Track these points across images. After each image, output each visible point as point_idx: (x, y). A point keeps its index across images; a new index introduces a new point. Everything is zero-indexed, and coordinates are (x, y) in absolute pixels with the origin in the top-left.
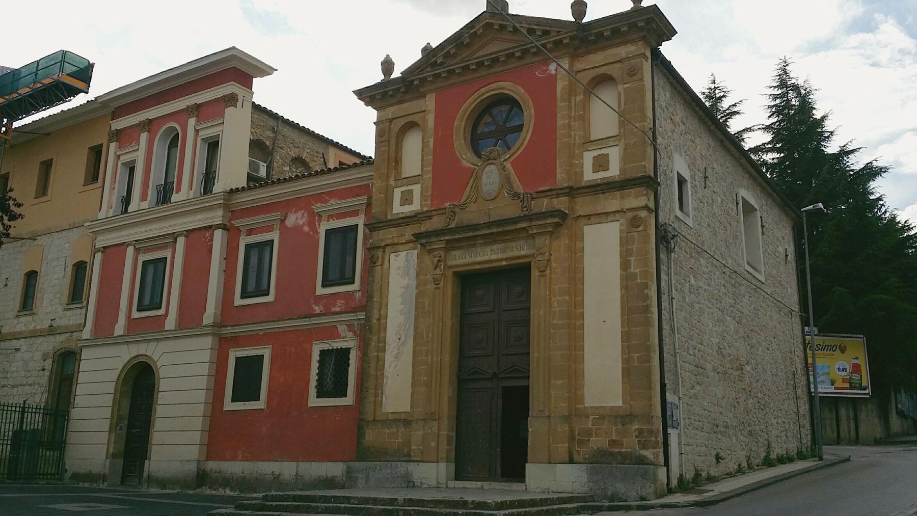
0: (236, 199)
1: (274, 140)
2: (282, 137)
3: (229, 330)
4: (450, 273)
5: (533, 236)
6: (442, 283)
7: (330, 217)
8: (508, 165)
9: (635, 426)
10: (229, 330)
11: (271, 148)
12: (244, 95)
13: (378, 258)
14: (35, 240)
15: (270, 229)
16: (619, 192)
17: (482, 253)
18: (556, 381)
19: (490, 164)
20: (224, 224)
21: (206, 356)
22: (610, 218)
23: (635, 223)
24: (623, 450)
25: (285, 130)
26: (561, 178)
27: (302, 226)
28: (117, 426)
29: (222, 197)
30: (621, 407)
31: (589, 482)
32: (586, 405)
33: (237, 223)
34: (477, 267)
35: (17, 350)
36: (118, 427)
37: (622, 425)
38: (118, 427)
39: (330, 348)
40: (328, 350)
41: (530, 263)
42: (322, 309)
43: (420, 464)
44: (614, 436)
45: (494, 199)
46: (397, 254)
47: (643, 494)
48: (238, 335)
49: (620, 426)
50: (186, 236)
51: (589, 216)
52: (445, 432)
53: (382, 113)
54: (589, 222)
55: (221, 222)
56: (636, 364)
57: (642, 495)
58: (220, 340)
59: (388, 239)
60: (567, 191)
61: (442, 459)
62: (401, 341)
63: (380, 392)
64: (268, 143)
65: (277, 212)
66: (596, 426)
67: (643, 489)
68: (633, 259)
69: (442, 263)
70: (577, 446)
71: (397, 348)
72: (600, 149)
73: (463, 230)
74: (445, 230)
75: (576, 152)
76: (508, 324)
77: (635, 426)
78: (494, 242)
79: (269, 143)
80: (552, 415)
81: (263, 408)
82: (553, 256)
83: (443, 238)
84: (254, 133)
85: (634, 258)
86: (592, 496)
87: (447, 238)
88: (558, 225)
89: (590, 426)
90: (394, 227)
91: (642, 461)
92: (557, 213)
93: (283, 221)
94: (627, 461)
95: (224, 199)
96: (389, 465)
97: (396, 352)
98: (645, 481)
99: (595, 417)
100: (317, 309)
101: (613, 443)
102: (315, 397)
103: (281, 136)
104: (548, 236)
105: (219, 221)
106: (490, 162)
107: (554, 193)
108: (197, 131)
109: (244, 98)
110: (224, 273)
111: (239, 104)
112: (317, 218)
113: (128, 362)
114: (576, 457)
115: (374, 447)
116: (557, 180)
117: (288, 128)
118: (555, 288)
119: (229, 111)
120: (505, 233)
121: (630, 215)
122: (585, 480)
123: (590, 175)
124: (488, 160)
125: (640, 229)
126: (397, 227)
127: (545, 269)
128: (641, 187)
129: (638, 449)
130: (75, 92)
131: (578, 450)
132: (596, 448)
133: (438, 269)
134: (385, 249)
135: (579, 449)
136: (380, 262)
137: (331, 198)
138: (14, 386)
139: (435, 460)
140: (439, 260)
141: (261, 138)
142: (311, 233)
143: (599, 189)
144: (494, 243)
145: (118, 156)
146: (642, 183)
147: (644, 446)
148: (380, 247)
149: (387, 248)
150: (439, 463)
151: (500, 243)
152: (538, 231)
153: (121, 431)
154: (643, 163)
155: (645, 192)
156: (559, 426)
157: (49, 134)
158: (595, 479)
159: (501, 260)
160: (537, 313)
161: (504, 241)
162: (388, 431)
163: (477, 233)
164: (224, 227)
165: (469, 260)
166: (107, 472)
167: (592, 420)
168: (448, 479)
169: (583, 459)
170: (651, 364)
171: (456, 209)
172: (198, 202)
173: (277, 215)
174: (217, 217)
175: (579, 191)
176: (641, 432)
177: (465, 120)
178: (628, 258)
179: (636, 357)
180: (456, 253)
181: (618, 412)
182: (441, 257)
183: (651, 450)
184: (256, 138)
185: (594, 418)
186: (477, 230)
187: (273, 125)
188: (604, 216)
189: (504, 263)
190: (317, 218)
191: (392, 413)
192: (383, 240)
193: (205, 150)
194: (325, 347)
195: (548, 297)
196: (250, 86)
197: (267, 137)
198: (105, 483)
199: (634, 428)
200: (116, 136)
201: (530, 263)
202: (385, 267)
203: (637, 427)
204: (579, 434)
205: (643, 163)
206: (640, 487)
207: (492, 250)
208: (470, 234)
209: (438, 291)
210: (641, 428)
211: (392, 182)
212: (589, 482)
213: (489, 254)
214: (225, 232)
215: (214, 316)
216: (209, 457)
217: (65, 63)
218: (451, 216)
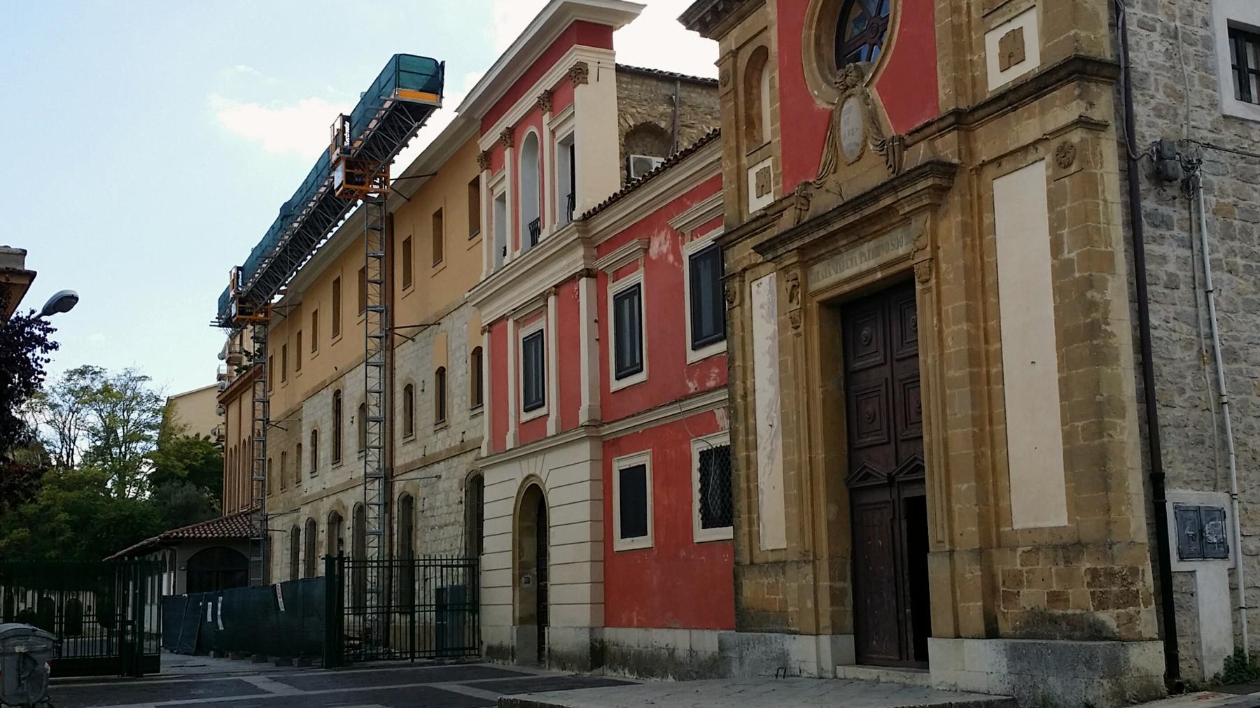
0: (594, 228)
1: (674, 117)
2: (689, 110)
3: (606, 430)
4: (813, 305)
5: (907, 218)
6: (802, 325)
7: (694, 234)
8: (873, 92)
9: (1086, 564)
10: (606, 430)
11: (670, 131)
12: (598, 61)
13: (735, 293)
14: (439, 324)
15: (633, 268)
16: (1036, 102)
17: (849, 263)
18: (959, 486)
19: (849, 96)
20: (587, 269)
21: (584, 472)
22: (1031, 158)
23: (1064, 158)
24: (1070, 612)
25: (693, 95)
26: (946, 98)
27: (667, 254)
28: (520, 578)
29: (575, 228)
30: (1065, 527)
31: (1010, 673)
32: (1015, 527)
33: (600, 265)
34: (847, 288)
35: (439, 477)
36: (523, 580)
37: (1066, 562)
38: (523, 580)
39: (710, 448)
40: (708, 450)
41: (912, 268)
42: (696, 385)
43: (797, 636)
44: (1054, 585)
45: (858, 160)
46: (759, 281)
47: (1090, 699)
48: (619, 435)
49: (1062, 566)
50: (555, 294)
51: (998, 160)
52: (826, 583)
53: (725, 44)
54: (1000, 171)
55: (583, 267)
56: (1082, 442)
57: (1087, 700)
58: (604, 446)
59: (744, 258)
60: (952, 119)
61: (825, 628)
62: (774, 429)
63: (755, 516)
64: (663, 125)
65: (632, 239)
66: (1027, 565)
67: (1090, 690)
68: (1065, 231)
69: (799, 290)
70: (1002, 605)
71: (769, 441)
72: (1009, 21)
73: (811, 227)
74: (797, 228)
75: (974, 37)
76: (904, 384)
77: (1086, 564)
78: (862, 240)
79: (666, 125)
80: (958, 548)
81: (650, 546)
82: (941, 249)
83: (791, 247)
84: (636, 115)
85: (1067, 229)
86: (1014, 699)
87: (796, 244)
88: (941, 192)
89: (1019, 567)
90: (749, 237)
91: (1097, 632)
92: (928, 168)
93: (646, 251)
94: (1078, 634)
95: (578, 231)
96: (763, 639)
97: (768, 449)
98: (1091, 673)
99: (1025, 549)
100: (692, 386)
101: (1055, 598)
102: (701, 526)
103: (686, 108)
104: (928, 214)
105: (580, 266)
106: (848, 93)
107: (934, 128)
108: (553, 132)
109: (600, 65)
110: (597, 343)
111: (591, 77)
112: (680, 238)
113: (522, 486)
114: (1004, 627)
115: (753, 608)
116: (940, 103)
117: (700, 90)
118: (948, 310)
119: (580, 92)
120: (870, 219)
121: (1055, 143)
122: (1004, 670)
123: (998, 80)
124: (846, 90)
125: (1073, 168)
126: (753, 236)
127: (928, 277)
128: (1069, 82)
129: (1092, 609)
130: (422, 113)
131: (1004, 612)
132: (1028, 608)
133: (795, 302)
134: (744, 277)
135: (1006, 611)
136: (737, 302)
137: (692, 203)
138: (441, 527)
139: (814, 633)
140: (794, 286)
141: (650, 119)
142: (676, 264)
143: (1005, 102)
144: (861, 241)
145: (492, 190)
146: (1070, 75)
147: (1101, 605)
148: (734, 274)
149: (748, 275)
150: (821, 637)
151: (870, 240)
152: (912, 207)
153: (527, 585)
154: (1072, 33)
155: (1077, 92)
156: (967, 568)
157: (435, 174)
158: (1018, 668)
159: (872, 271)
160: (927, 360)
161: (876, 235)
162: (766, 582)
163: (830, 229)
164: (589, 273)
165: (834, 278)
166: (515, 644)
167: (1020, 555)
168: (837, 663)
169: (1013, 629)
170: (1106, 439)
171: (811, 190)
172: (554, 242)
173: (634, 245)
174: (575, 261)
175: (976, 116)
176: (1094, 573)
177: (814, 24)
178: (1059, 232)
179: (1080, 429)
180: (818, 268)
181: (1061, 537)
182: (796, 279)
183: (1111, 610)
184: (641, 121)
185: (1024, 552)
186: (828, 223)
187: (670, 94)
188: (1020, 155)
189: (879, 275)
190: (680, 238)
191: (772, 550)
192: (739, 262)
193: (567, 160)
194: (704, 446)
195: (936, 329)
196: (609, 45)
197: (659, 114)
198: (515, 660)
199: (1083, 569)
200: (486, 161)
201: (912, 268)
202: (747, 306)
203: (1088, 565)
204: (1004, 583)
205: (1072, 33)
206: (1084, 686)
207: (862, 255)
208: (822, 233)
209: (799, 339)
210: (1094, 569)
211: (744, 161)
212: (1010, 673)
213: (858, 262)
214: (592, 281)
215: (589, 410)
216: (608, 623)
217: (401, 73)
218: (802, 204)
